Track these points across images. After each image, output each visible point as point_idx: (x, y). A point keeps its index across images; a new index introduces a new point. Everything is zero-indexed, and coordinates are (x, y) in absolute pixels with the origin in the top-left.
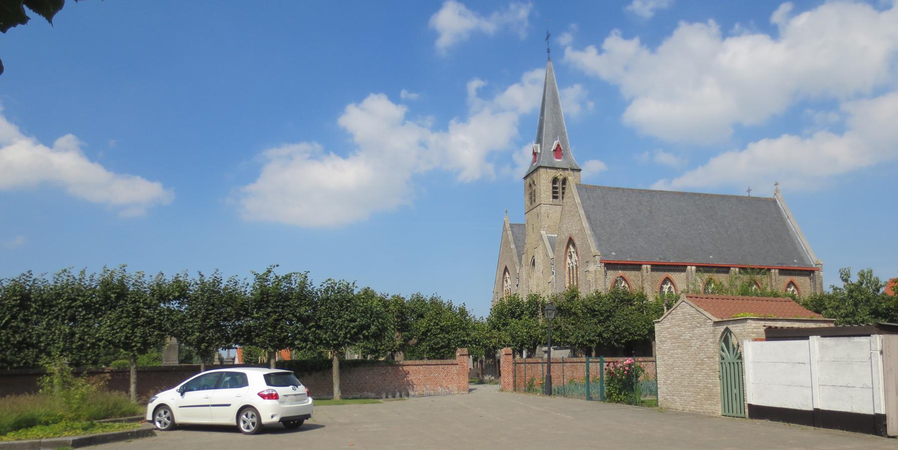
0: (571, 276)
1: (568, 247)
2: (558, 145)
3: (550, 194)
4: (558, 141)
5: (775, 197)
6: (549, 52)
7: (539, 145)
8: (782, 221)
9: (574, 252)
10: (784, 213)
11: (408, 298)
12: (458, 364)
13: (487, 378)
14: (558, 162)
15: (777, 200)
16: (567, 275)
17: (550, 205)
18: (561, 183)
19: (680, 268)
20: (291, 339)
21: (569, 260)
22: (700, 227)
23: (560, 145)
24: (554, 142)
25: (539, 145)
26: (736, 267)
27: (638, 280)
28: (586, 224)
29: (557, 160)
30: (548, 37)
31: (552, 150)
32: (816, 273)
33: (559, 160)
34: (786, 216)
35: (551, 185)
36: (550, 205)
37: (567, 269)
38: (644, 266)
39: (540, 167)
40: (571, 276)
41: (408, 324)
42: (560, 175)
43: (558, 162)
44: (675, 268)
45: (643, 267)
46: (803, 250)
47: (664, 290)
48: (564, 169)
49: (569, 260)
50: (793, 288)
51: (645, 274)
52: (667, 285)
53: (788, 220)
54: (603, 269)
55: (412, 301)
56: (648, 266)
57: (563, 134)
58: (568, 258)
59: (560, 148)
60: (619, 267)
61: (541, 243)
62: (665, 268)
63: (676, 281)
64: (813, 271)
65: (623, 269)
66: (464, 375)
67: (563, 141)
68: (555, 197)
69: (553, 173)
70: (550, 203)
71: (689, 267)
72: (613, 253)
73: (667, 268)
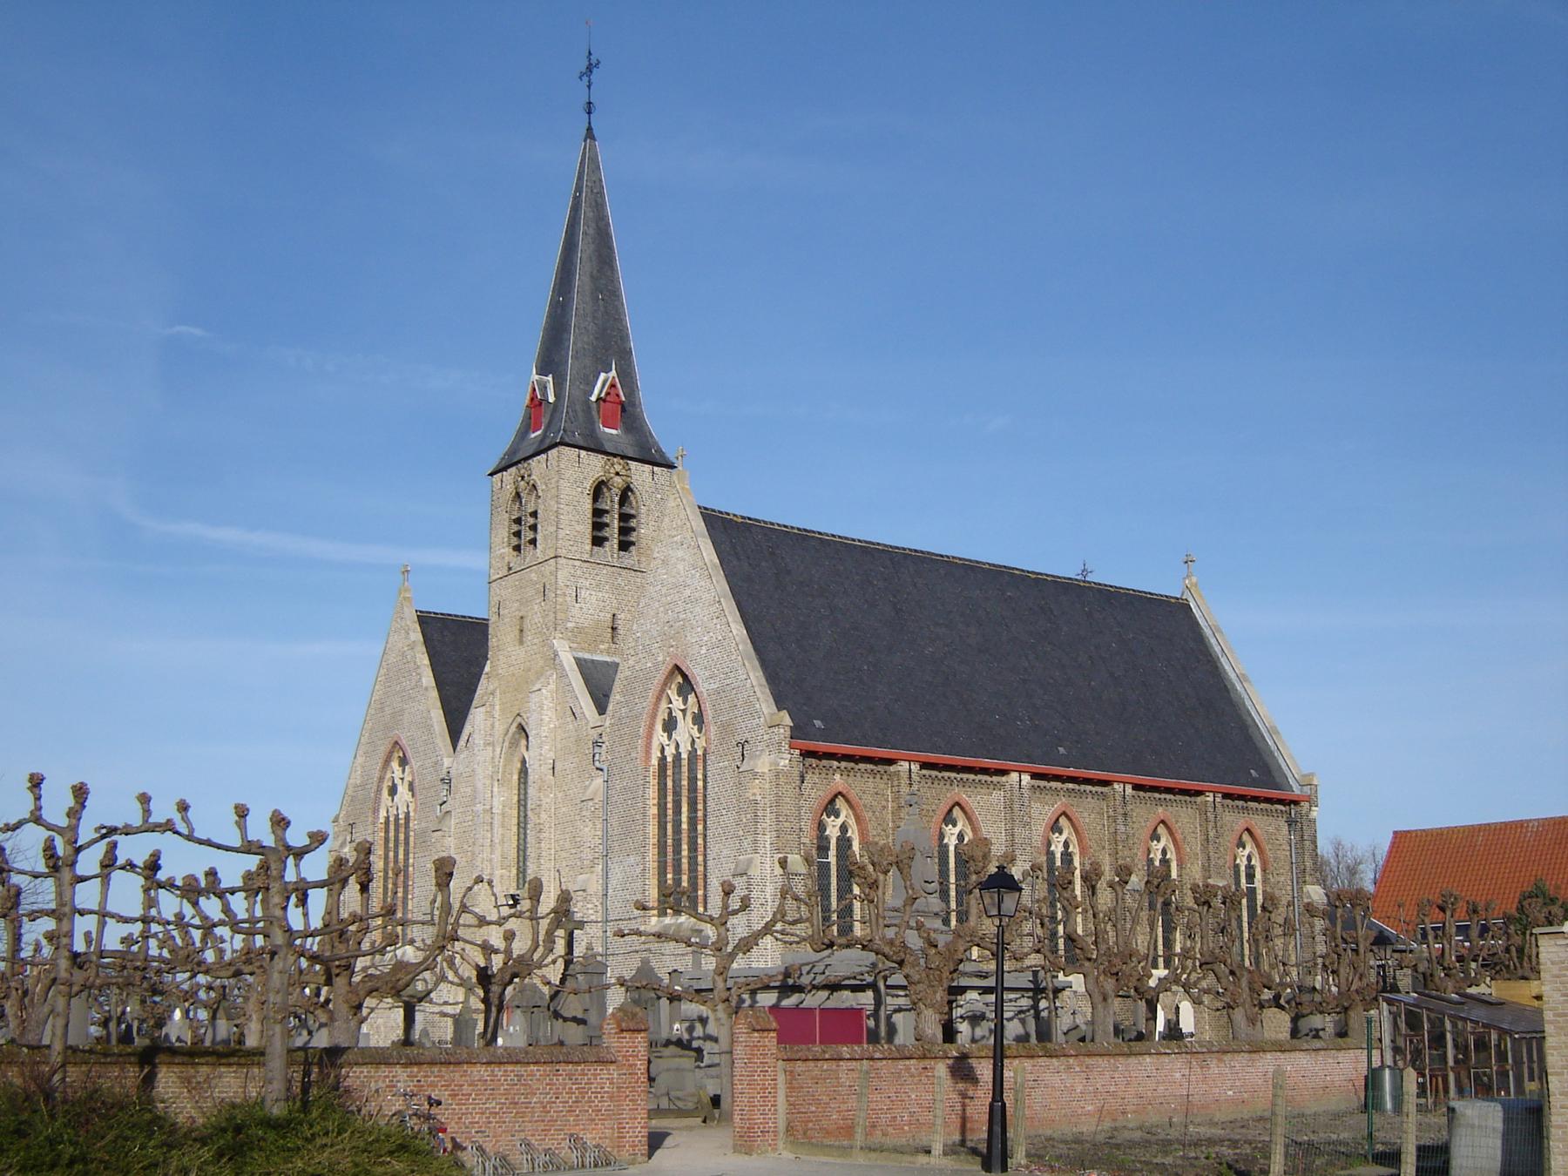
2: (613, 386)
3: (586, 529)
4: (613, 373)
5: (1187, 596)
6: (589, 113)
7: (550, 378)
8: (1209, 661)
16: (653, 782)
20: (1422, 952)
23: (619, 386)
25: (550, 378)
27: (884, 807)
30: (590, 69)
31: (593, 398)
34: (1217, 649)
47: (827, 833)
49: (660, 736)
53: (1223, 660)
57: (624, 356)
67: (627, 375)
68: (598, 541)
70: (586, 557)
72: (818, 723)
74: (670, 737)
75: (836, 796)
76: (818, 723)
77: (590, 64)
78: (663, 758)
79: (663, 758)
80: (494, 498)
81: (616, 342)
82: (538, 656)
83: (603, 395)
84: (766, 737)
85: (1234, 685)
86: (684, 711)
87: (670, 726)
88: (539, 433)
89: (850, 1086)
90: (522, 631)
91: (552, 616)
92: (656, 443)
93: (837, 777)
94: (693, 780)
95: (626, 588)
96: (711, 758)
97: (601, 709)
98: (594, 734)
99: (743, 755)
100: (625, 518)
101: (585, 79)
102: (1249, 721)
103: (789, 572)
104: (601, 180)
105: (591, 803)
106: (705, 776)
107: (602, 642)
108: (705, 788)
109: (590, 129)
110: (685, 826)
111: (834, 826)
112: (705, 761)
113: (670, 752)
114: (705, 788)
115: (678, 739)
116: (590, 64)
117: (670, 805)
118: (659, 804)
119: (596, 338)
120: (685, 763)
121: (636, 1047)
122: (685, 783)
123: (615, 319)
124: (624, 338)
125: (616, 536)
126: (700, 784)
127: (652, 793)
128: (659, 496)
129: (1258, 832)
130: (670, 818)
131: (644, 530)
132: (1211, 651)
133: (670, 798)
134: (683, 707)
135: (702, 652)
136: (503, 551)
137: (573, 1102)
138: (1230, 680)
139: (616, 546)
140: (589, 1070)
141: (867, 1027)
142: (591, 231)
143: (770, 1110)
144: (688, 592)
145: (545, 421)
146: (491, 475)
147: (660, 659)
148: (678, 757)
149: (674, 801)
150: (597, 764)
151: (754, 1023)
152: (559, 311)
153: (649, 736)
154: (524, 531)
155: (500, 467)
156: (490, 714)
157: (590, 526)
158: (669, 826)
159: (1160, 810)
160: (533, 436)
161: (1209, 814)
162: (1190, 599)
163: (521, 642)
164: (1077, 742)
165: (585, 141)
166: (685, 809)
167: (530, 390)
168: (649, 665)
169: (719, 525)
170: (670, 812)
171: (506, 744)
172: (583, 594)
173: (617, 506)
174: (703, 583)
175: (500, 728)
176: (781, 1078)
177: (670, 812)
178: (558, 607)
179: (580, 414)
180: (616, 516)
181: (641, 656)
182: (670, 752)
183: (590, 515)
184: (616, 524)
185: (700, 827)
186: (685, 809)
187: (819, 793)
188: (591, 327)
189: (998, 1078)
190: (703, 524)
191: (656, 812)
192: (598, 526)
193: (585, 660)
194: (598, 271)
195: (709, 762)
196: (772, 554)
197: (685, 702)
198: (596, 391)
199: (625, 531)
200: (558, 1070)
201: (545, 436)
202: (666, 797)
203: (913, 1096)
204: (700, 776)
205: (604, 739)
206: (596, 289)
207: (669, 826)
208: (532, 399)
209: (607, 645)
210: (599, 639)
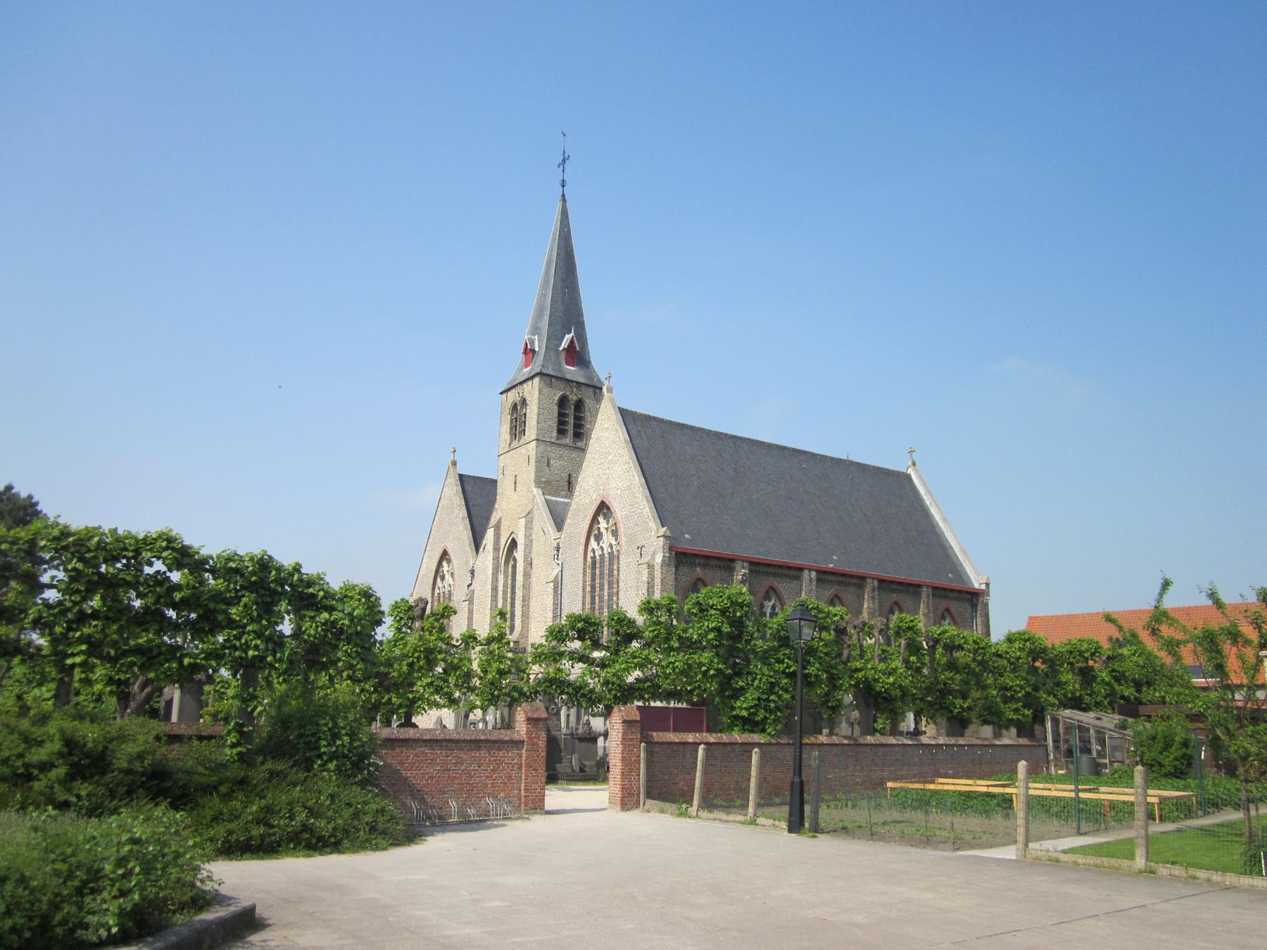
1: (594, 520)
5: (910, 471)
6: (563, 186)
7: (536, 337)
12: (570, 475)
13: (719, 802)
21: (593, 544)
24: (563, 337)
29: (568, 367)
30: (564, 161)
31: (561, 349)
33: (572, 368)
35: (556, 408)
38: (738, 565)
41: (129, 693)
44: (785, 572)
52: (770, 601)
60: (697, 561)
63: (785, 596)
65: (704, 566)
66: (536, 770)
68: (561, 432)
72: (687, 536)
74: (598, 544)
75: (697, 580)
76: (687, 536)
78: (594, 558)
79: (594, 558)
84: (655, 543)
85: (938, 524)
86: (607, 529)
87: (599, 538)
92: (597, 375)
93: (698, 569)
94: (611, 571)
102: (947, 546)
106: (618, 568)
107: (563, 490)
109: (563, 196)
112: (618, 559)
120: (607, 560)
122: (606, 572)
124: (580, 314)
129: (953, 610)
137: (491, 770)
144: (610, 458)
146: (501, 393)
147: (594, 497)
148: (602, 556)
155: (509, 386)
157: (556, 422)
159: (894, 595)
167: (524, 344)
169: (624, 413)
182: (598, 553)
184: (572, 421)
188: (561, 308)
196: (663, 437)
198: (563, 345)
204: (615, 567)
207: (597, 598)
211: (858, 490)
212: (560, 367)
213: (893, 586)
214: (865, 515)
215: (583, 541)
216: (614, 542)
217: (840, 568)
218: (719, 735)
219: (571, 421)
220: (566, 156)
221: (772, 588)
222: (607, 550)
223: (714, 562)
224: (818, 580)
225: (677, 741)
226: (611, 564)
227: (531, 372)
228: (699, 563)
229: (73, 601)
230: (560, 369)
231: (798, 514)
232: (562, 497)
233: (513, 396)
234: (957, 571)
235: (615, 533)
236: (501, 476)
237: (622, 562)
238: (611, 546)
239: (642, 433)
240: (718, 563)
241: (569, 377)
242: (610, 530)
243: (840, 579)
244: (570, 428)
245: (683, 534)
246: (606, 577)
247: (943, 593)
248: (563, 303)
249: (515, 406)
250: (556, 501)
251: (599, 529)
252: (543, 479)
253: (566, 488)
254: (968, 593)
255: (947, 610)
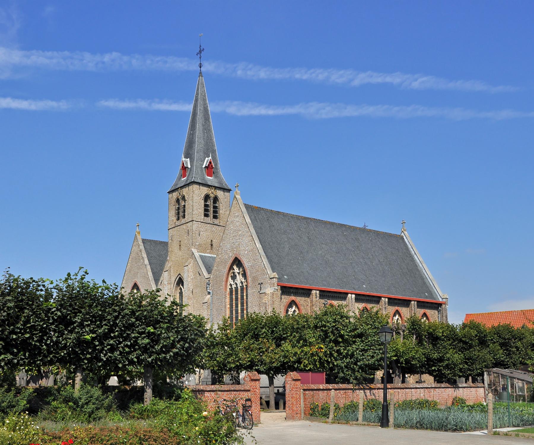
0: (234, 297)
1: (231, 268)
2: (210, 163)
3: (202, 211)
4: (210, 158)
5: (402, 234)
7: (188, 159)
8: (410, 257)
9: (239, 273)
10: (412, 250)
11: (516, 328)
14: (210, 180)
15: (404, 237)
16: (228, 296)
17: (202, 222)
18: (212, 201)
19: (306, 292)
22: (351, 257)
25: (188, 159)
26: (386, 298)
28: (259, 245)
30: (200, 51)
31: (204, 166)
32: (443, 306)
34: (413, 252)
35: (203, 202)
36: (202, 222)
37: (228, 290)
38: (314, 292)
39: (194, 183)
40: (234, 297)
42: (212, 192)
43: (210, 180)
44: (337, 295)
45: (312, 292)
46: (430, 284)
48: (216, 188)
49: (230, 281)
50: (397, 317)
51: (314, 299)
53: (415, 256)
54: (280, 292)
55: (464, 326)
56: (317, 291)
57: (214, 152)
58: (230, 279)
59: (212, 166)
61: (191, 261)
62: (333, 295)
64: (440, 305)
67: (214, 158)
68: (206, 215)
69: (205, 190)
71: (349, 295)
72: (285, 277)
73: (332, 295)
74: (234, 281)
76: (285, 277)
77: (201, 50)
78: (231, 289)
80: (170, 200)
81: (211, 147)
82: (186, 254)
83: (207, 165)
87: (234, 277)
88: (185, 178)
89: (323, 398)
90: (180, 246)
91: (191, 241)
95: (216, 231)
96: (249, 289)
97: (209, 272)
98: (207, 281)
99: (261, 288)
100: (215, 207)
101: (199, 55)
103: (273, 226)
104: (205, 90)
105: (206, 304)
108: (247, 298)
110: (239, 311)
111: (291, 312)
113: (234, 286)
114: (247, 298)
115: (237, 282)
116: (201, 50)
117: (234, 304)
118: (230, 304)
119: (204, 146)
121: (256, 385)
123: (210, 139)
125: (212, 213)
126: (245, 297)
127: (228, 300)
128: (226, 200)
129: (428, 314)
130: (234, 309)
131: (222, 211)
132: (411, 253)
133: (234, 302)
134: (238, 271)
135: (246, 253)
136: (173, 218)
138: (418, 263)
139: (212, 217)
140: (241, 393)
141: (518, 387)
142: (202, 109)
143: (298, 406)
144: (240, 233)
145: (187, 174)
147: (231, 255)
148: (236, 289)
149: (235, 303)
150: (208, 291)
151: (293, 377)
152: (191, 136)
153: (227, 281)
154: (181, 213)
155: (173, 189)
156: (170, 275)
157: (203, 210)
158: (234, 311)
160: (183, 179)
161: (412, 308)
162: (404, 236)
163: (180, 249)
164: (369, 283)
165: (199, 77)
166: (239, 305)
168: (227, 257)
170: (234, 307)
171: (175, 283)
172: (201, 233)
173: (212, 203)
174: (246, 230)
175: (173, 279)
176: (302, 395)
177: (234, 307)
178: (193, 237)
179: (199, 172)
180: (212, 207)
181: (223, 254)
182: (234, 286)
183: (203, 206)
184: (212, 209)
185: (245, 312)
186: (239, 305)
187: (286, 300)
189: (385, 396)
190: (245, 209)
191: (229, 307)
192: (206, 210)
193: (202, 256)
194: (205, 123)
195: (248, 290)
196: (268, 220)
197: (239, 270)
199: (215, 212)
200: (231, 393)
201: (187, 179)
202: (232, 301)
203: (342, 401)
204: (245, 295)
205: (211, 282)
206: (204, 129)
207: (234, 311)
208: (182, 167)
209: (209, 251)
210: (207, 248)
211: (375, 247)
212: (204, 178)
213: (396, 301)
214: (379, 261)
215: (224, 279)
216: (243, 280)
217: (368, 293)
218: (333, 385)
219: (211, 209)
220: (202, 49)
221: (397, 311)
222: (239, 285)
223: (301, 291)
224: (320, 295)
225: (316, 388)
226: (242, 292)
227: (187, 181)
228: (293, 292)
229: (356, 348)
230: (204, 179)
231: (343, 262)
232: (208, 253)
233: (175, 195)
234: (430, 291)
235: (244, 275)
236: (170, 241)
237: (249, 291)
238: (242, 283)
239: (257, 218)
240: (302, 291)
241: (209, 183)
242: (241, 274)
243: (368, 298)
244: (211, 214)
245: (283, 275)
246: (239, 300)
247: (422, 304)
248: (204, 139)
249: (178, 201)
250: (205, 256)
251: (234, 273)
252: (197, 244)
253: (210, 248)
254: (436, 304)
255: (397, 311)
